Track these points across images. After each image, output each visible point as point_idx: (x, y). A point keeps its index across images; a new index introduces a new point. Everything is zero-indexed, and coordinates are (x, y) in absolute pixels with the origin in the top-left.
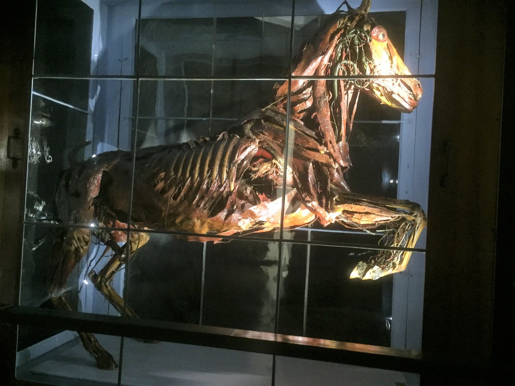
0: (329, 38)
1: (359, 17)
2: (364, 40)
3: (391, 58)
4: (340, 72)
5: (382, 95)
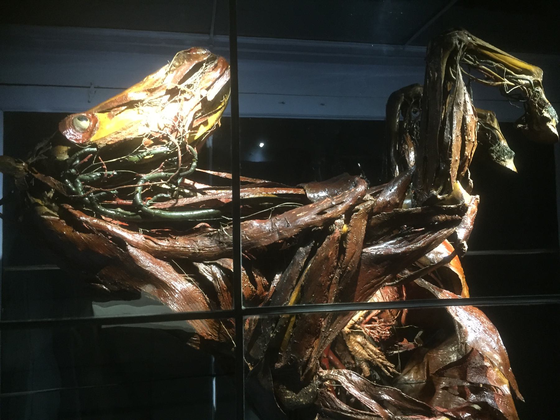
0: (83, 236)
1: (36, 173)
2: (91, 159)
3: (131, 104)
4: (160, 207)
5: (206, 123)
